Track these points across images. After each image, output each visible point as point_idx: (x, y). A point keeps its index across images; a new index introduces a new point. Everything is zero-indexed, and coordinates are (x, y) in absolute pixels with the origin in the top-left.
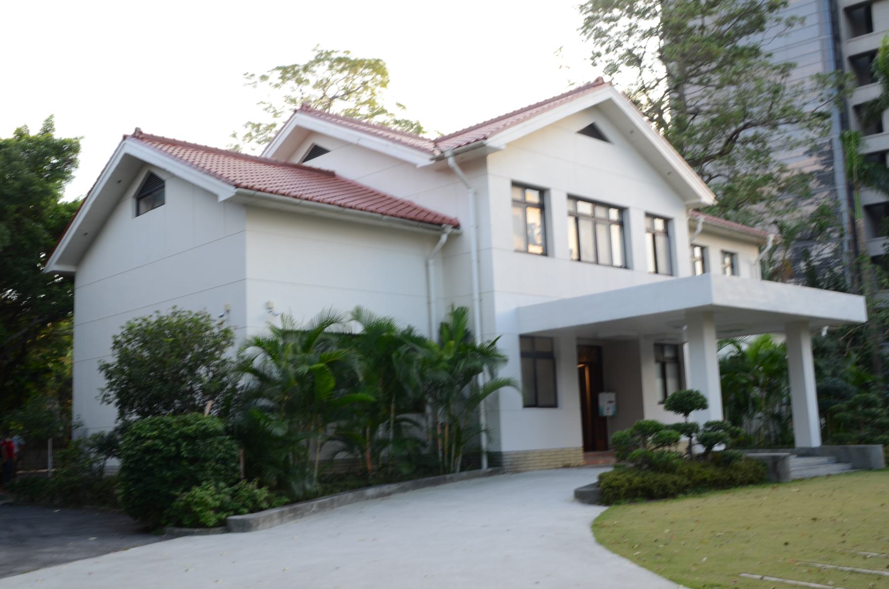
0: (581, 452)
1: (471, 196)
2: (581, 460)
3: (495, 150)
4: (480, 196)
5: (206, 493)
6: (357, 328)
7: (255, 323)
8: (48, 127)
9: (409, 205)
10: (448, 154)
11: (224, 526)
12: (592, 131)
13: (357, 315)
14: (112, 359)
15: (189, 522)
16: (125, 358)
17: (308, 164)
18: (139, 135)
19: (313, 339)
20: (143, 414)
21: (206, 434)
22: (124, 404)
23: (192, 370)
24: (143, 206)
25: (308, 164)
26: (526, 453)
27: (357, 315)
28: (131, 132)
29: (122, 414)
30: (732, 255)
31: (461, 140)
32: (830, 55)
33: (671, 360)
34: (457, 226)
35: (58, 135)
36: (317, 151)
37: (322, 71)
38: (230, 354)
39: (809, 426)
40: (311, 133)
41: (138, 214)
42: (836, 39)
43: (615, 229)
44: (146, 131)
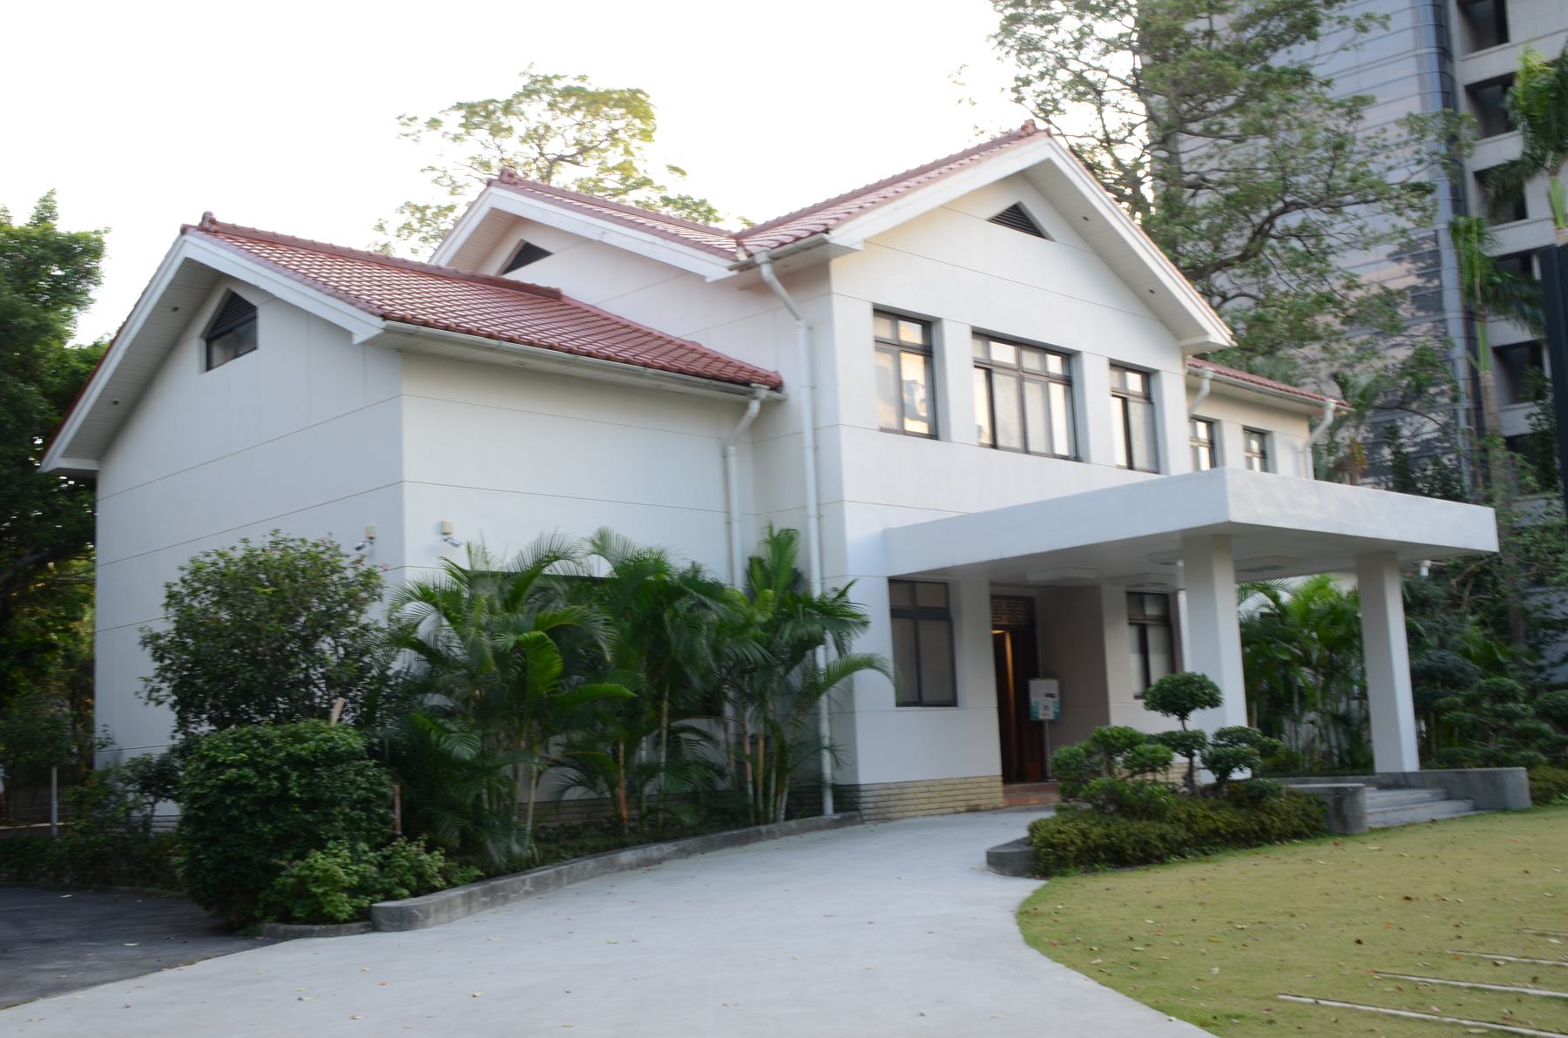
0: (999, 784)
1: (802, 332)
2: (999, 799)
3: (846, 251)
4: (819, 332)
5: (334, 862)
6: (602, 568)
7: (419, 559)
8: (46, 212)
9: (692, 349)
10: (760, 258)
11: (366, 921)
12: (1015, 218)
13: (601, 545)
14: (164, 624)
15: (305, 913)
16: (187, 623)
17: (513, 276)
18: (210, 226)
19: (522, 587)
20: (221, 723)
21: (332, 757)
22: (187, 704)
23: (307, 643)
24: (217, 352)
25: (513, 276)
26: (902, 786)
27: (601, 545)
28: (196, 221)
29: (183, 723)
30: (1262, 434)
31: (784, 234)
32: (1434, 83)
33: (1157, 619)
34: (777, 386)
35: (66, 224)
36: (528, 254)
37: (536, 112)
38: (375, 614)
39: (1398, 735)
40: (518, 221)
41: (209, 366)
42: (1445, 53)
43: (1057, 391)
44: (219, 219)
